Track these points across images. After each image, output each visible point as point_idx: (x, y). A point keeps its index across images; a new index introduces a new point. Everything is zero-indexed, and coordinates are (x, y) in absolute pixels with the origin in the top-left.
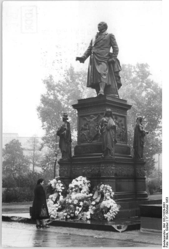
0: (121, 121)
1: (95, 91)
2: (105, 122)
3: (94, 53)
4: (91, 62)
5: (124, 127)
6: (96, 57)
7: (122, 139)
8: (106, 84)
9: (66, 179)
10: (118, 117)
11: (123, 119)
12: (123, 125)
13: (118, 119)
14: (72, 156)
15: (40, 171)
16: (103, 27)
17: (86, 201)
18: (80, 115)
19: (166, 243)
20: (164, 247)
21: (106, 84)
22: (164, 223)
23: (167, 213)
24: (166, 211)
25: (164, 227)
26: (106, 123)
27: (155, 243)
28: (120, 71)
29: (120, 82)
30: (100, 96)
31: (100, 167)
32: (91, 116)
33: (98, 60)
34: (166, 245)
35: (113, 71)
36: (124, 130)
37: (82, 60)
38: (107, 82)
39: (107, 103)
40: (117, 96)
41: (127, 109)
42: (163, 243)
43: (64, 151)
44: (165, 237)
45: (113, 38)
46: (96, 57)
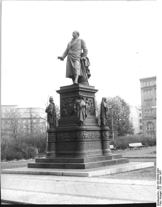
0: (90, 101)
1: (71, 80)
2: (79, 103)
3: (70, 54)
4: (69, 60)
5: (93, 105)
6: (72, 57)
7: (92, 113)
8: (79, 76)
9: (53, 142)
10: (88, 98)
11: (92, 99)
12: (92, 103)
13: (88, 100)
14: (129, 144)
16: (76, 35)
18: (62, 97)
19: (159, 202)
21: (79, 76)
23: (160, 184)
26: (79, 104)
28: (89, 66)
29: (89, 74)
30: (75, 84)
31: (76, 133)
32: (69, 98)
33: (73, 59)
34: (159, 203)
36: (93, 107)
37: (62, 59)
38: (79, 75)
39: (80, 89)
40: (87, 83)
41: (95, 93)
43: (51, 123)
44: (158, 197)
45: (83, 43)
46: (72, 57)
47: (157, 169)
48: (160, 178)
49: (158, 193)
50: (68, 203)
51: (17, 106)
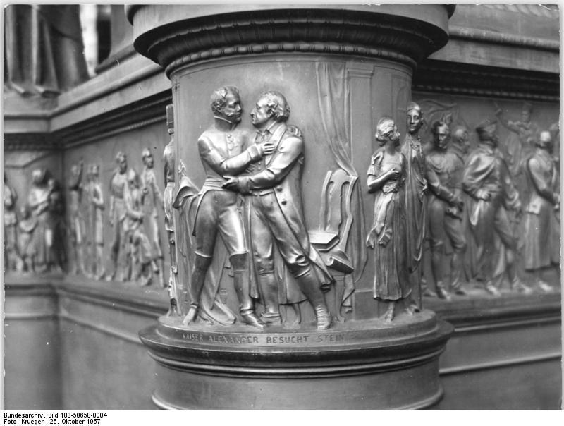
15: (524, 246)
17: (141, 232)
19: (13, 419)
20: (5, 415)
23: (64, 422)
24: (68, 419)
27: (352, 200)
34: (10, 419)
35: (174, 216)
42: (14, 412)
44: (28, 416)
48: (80, 422)
49: (38, 416)
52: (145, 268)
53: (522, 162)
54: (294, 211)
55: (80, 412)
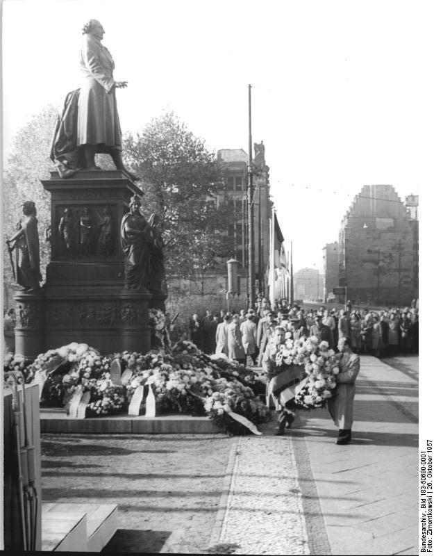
19: (427, 543)
20: (423, 551)
22: (424, 497)
23: (429, 476)
25: (423, 507)
34: (427, 546)
42: (421, 542)
44: (424, 529)
47: (420, 454)
48: (430, 460)
49: (424, 519)
50: (147, 527)
51: (94, 31)
52: (258, 542)
53: (195, 246)
54: (332, 325)
55: (420, 477)
